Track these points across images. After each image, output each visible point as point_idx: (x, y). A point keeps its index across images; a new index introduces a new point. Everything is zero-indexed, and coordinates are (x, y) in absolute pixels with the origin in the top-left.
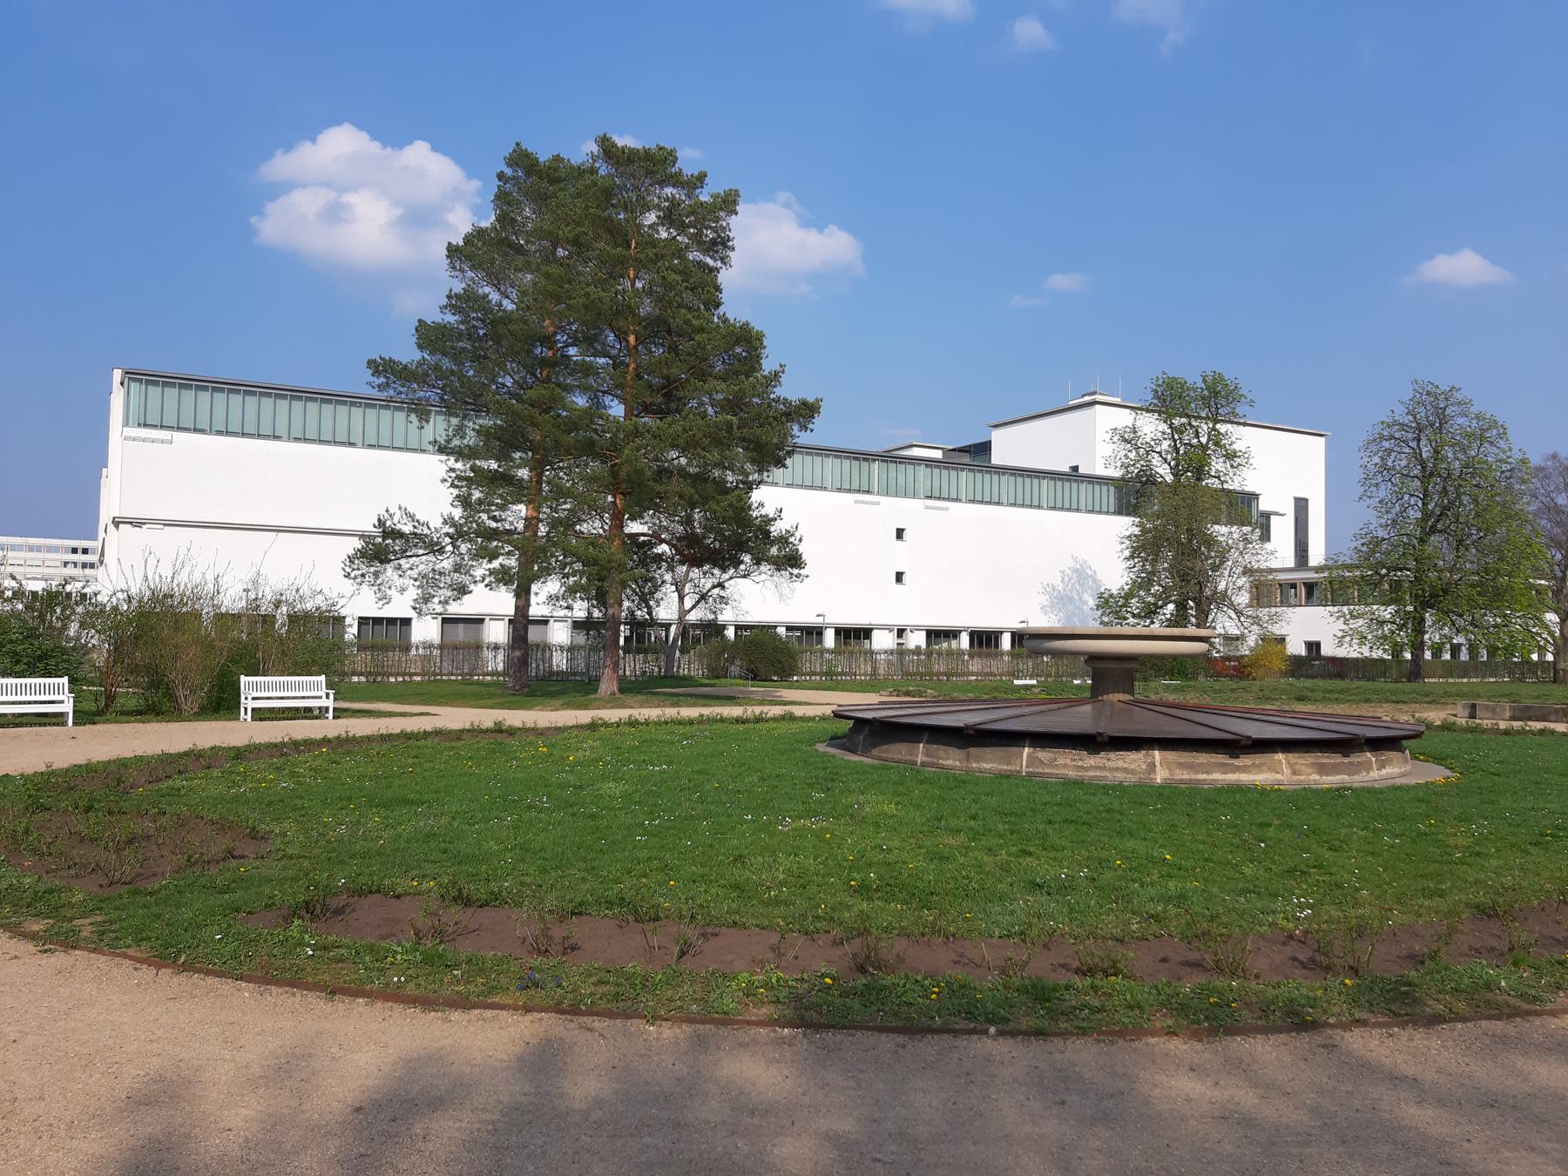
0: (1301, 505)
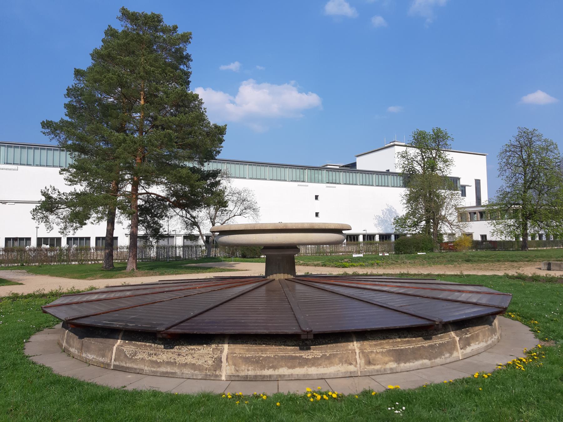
0: (478, 182)
